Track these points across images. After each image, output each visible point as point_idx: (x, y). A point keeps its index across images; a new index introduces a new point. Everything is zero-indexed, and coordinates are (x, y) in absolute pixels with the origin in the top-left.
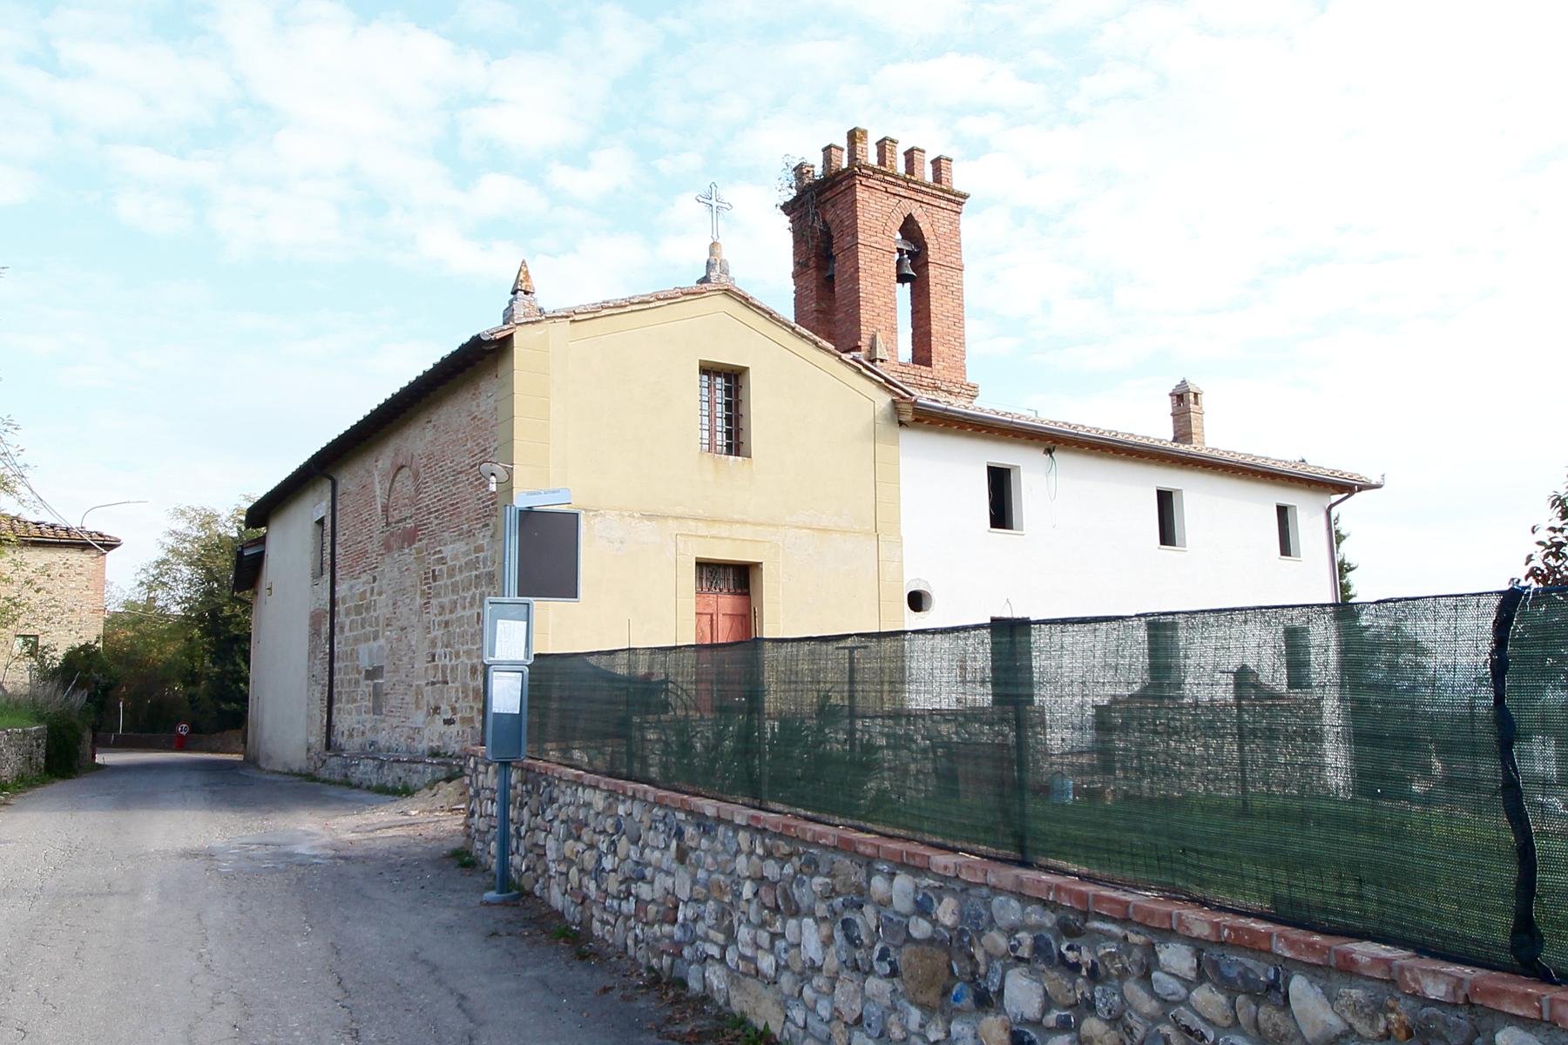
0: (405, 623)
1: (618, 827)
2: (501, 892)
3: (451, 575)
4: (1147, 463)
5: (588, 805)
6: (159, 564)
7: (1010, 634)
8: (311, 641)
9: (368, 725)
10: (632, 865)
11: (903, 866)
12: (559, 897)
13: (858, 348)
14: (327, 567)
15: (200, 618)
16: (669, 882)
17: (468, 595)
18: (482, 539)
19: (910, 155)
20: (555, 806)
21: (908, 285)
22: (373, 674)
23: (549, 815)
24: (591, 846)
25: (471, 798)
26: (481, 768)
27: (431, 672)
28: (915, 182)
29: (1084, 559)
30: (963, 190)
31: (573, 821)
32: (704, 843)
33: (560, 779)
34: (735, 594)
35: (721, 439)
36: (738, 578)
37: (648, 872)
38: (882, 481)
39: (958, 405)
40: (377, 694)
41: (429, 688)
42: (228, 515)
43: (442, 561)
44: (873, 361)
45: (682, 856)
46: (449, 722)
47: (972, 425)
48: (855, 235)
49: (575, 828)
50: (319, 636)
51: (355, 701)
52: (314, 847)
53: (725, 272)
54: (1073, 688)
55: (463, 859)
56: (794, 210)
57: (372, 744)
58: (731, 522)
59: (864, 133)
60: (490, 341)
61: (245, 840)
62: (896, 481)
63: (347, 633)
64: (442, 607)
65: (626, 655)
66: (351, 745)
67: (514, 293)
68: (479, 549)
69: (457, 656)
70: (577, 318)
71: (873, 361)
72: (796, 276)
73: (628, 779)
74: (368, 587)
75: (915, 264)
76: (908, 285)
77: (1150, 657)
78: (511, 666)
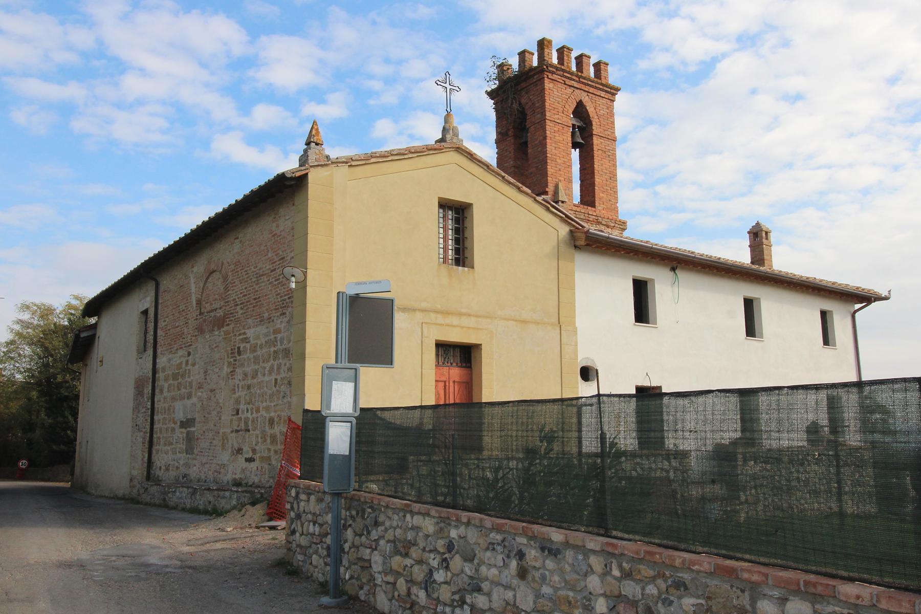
0: (214, 387)
1: (450, 547)
2: (335, 597)
3: (254, 349)
4: (737, 279)
5: (416, 529)
6: (8, 344)
9: (182, 462)
10: (466, 579)
11: (797, 592)
12: (386, 602)
13: (546, 193)
14: (150, 345)
15: (39, 384)
16: (509, 595)
19: (580, 59)
20: (381, 528)
22: (187, 423)
23: (374, 535)
24: (420, 562)
25: (292, 521)
26: (303, 497)
28: (584, 78)
29: (698, 349)
30: (617, 85)
31: (400, 541)
32: (550, 564)
33: (387, 507)
34: (461, 367)
36: (462, 355)
37: (485, 586)
38: (564, 288)
39: (615, 234)
40: (190, 439)
41: (234, 435)
42: (61, 309)
43: (246, 340)
44: (557, 202)
45: (522, 574)
47: (624, 249)
48: (543, 114)
49: (403, 548)
51: (172, 444)
52: (162, 559)
53: (456, 134)
55: (286, 568)
56: (498, 95)
57: (185, 476)
58: (460, 314)
60: (291, 179)
61: (105, 553)
62: (572, 287)
63: (165, 394)
64: (246, 375)
66: (168, 477)
67: (308, 143)
69: (258, 410)
70: (353, 163)
73: (454, 507)
74: (184, 360)
75: (584, 134)
77: (829, 413)
78: (342, 418)
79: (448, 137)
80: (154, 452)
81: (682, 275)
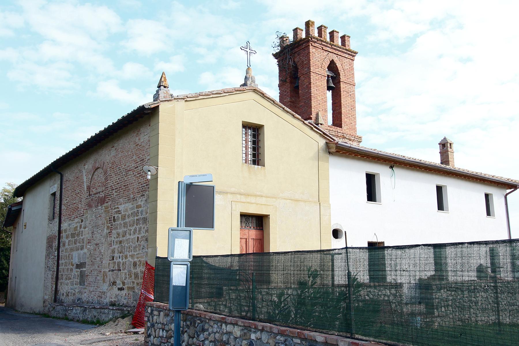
0: (98, 242)
3: (124, 218)
5: (229, 333)
7: (375, 247)
8: (47, 250)
9: (77, 291)
13: (311, 118)
17: (133, 228)
18: (141, 202)
19: (332, 34)
20: (206, 333)
21: (331, 91)
22: (80, 266)
23: (202, 337)
26: (156, 313)
27: (112, 265)
34: (256, 229)
35: (250, 157)
36: (258, 222)
38: (321, 178)
39: (354, 145)
40: (82, 276)
41: (111, 273)
43: (119, 212)
44: (317, 124)
46: (120, 289)
47: (360, 154)
48: (309, 68)
50: (52, 248)
51: (70, 279)
53: (253, 81)
54: (406, 274)
56: (280, 56)
57: (79, 299)
58: (256, 196)
59: (313, 23)
60: (148, 109)
62: (327, 179)
63: (67, 246)
64: (118, 234)
65: (319, 255)
67: (159, 87)
68: (139, 207)
69: (126, 257)
70: (188, 99)
71: (317, 124)
72: (280, 86)
74: (78, 225)
76: (331, 91)
78: (181, 262)
79: (249, 83)
80: (59, 284)
81: (399, 172)
